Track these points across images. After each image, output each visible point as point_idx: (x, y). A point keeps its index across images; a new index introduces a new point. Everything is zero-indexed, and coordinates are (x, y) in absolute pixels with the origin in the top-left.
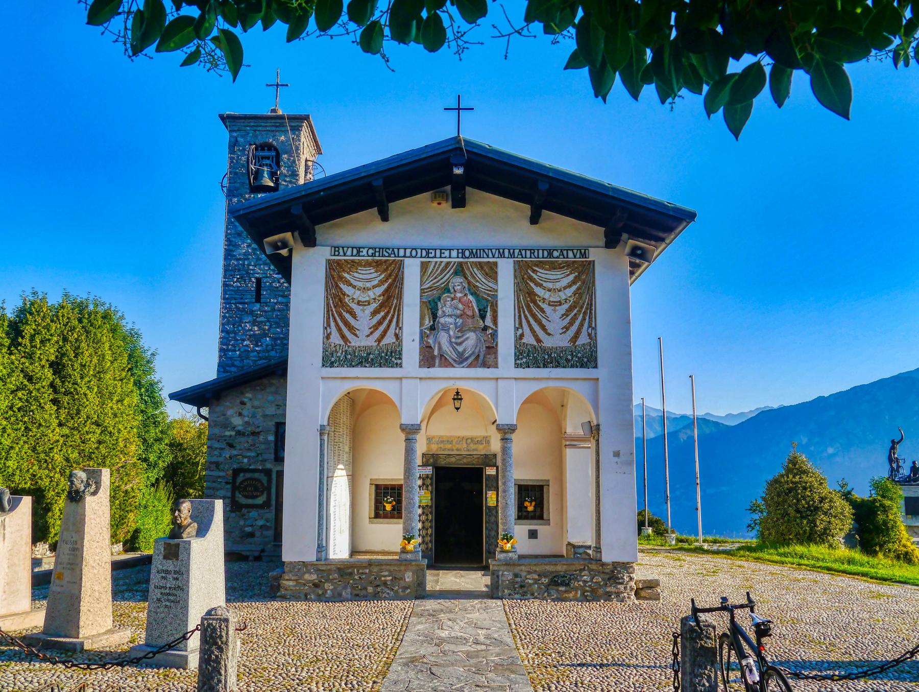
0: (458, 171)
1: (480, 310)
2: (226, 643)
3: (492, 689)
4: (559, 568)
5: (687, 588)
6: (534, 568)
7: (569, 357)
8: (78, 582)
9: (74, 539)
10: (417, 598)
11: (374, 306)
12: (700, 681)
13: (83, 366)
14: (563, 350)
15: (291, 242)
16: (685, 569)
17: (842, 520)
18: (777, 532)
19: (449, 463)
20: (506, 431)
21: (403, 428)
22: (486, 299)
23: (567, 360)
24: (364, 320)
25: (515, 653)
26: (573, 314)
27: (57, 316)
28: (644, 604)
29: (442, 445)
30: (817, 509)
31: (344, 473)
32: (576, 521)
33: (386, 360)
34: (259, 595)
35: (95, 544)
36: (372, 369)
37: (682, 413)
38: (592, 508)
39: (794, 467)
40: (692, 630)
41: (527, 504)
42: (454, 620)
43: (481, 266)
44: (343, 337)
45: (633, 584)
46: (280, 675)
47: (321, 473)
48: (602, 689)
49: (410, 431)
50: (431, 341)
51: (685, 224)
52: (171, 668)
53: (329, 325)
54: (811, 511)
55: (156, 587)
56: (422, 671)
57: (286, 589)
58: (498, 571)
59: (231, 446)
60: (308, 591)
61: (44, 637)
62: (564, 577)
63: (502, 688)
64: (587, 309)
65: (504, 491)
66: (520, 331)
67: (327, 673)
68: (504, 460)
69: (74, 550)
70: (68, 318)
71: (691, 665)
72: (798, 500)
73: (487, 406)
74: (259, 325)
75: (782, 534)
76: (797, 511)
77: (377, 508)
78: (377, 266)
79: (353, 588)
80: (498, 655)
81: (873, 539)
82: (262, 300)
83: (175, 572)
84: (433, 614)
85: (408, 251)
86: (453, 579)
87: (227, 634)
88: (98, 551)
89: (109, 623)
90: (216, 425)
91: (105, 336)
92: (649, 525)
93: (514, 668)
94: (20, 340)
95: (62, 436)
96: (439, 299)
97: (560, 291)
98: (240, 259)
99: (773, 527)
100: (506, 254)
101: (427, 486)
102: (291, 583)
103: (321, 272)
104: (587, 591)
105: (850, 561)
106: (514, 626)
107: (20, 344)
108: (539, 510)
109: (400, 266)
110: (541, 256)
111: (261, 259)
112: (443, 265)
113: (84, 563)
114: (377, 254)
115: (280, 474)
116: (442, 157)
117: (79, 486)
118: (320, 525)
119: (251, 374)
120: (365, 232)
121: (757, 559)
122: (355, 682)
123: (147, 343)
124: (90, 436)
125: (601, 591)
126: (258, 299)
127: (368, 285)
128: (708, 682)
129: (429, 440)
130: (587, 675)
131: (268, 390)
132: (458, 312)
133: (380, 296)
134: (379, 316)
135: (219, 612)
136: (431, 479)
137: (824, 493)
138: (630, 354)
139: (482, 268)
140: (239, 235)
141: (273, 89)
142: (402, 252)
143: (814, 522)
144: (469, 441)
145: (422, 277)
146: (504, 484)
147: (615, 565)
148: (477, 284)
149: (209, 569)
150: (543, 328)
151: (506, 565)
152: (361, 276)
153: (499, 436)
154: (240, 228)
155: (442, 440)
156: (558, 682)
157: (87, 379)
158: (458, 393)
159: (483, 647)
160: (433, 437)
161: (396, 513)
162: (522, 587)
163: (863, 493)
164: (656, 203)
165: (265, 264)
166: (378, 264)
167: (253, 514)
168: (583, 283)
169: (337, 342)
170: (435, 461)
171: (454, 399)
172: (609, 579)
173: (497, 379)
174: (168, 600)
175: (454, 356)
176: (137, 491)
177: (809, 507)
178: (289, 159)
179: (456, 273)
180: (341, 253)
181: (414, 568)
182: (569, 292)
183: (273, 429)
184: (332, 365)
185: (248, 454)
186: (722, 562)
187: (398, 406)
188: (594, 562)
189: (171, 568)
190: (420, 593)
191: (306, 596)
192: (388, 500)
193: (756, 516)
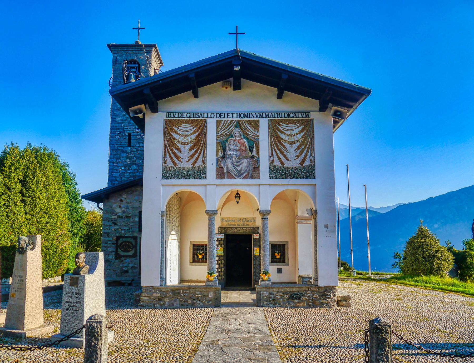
0: (237, 69)
1: (249, 147)
2: (101, 336)
3: (258, 361)
4: (294, 290)
5: (365, 300)
6: (281, 290)
7: (300, 173)
8: (23, 299)
9: (21, 275)
10: (216, 306)
11: (191, 145)
12: (382, 358)
13: (37, 182)
14: (296, 168)
15: (144, 110)
16: (362, 289)
17: (448, 262)
18: (412, 269)
19: (234, 232)
20: (265, 214)
21: (207, 213)
22: (253, 141)
23: (298, 174)
24: (185, 153)
25: (270, 339)
26: (301, 149)
27: (24, 156)
28: (342, 309)
29: (229, 223)
30: (434, 256)
31: (175, 237)
32: (303, 264)
33: (198, 175)
34: (128, 305)
35: (33, 277)
36: (190, 180)
37: (357, 206)
38: (311, 257)
39: (421, 234)
40: (377, 328)
41: (276, 254)
42: (235, 319)
43: (250, 122)
44: (174, 162)
45: (335, 298)
46: (136, 352)
47: (162, 238)
48: (322, 361)
49: (211, 214)
50: (222, 164)
51: (365, 97)
52: (74, 348)
53: (166, 156)
54: (431, 258)
55: (66, 302)
56: (217, 350)
57: (143, 302)
58: (261, 291)
59: (115, 224)
60: (155, 303)
61: (4, 329)
62: (297, 294)
63: (263, 360)
64: (309, 146)
65: (264, 247)
66: (272, 159)
67: (163, 351)
68: (263, 230)
69: (21, 280)
70: (29, 157)
71: (376, 349)
72: (424, 252)
73: (254, 201)
74: (130, 158)
75: (415, 270)
76: (423, 258)
77: (194, 257)
78: (192, 123)
79: (180, 301)
80: (261, 339)
81: (465, 273)
82: (132, 145)
83: (76, 293)
84: (224, 316)
85: (209, 115)
86: (236, 295)
87: (101, 330)
88: (35, 281)
89: (42, 321)
90: (107, 213)
91: (49, 166)
92: (345, 267)
93: (270, 347)
94: (3, 168)
95: (27, 219)
96: (227, 141)
97: (294, 136)
98: (119, 123)
99: (410, 266)
100: (264, 116)
101: (221, 245)
102: (146, 298)
103: (160, 127)
104: (310, 302)
105: (453, 285)
106: (270, 322)
107: (4, 171)
108: (282, 258)
109: (205, 123)
110: (283, 116)
111: (131, 123)
112: (229, 122)
113: (27, 288)
114: (192, 116)
115: (141, 238)
116: (229, 60)
117: (23, 245)
118: (162, 266)
119: (125, 185)
120: (185, 104)
121: (402, 284)
122: (178, 357)
123: (71, 169)
124: (42, 219)
125: (318, 302)
126: (129, 145)
127: (187, 133)
128: (386, 358)
129: (222, 219)
130: (313, 352)
131: (135, 193)
132: (238, 148)
133: (194, 140)
134: (193, 151)
135: (96, 318)
136: (224, 241)
137: (438, 248)
138: (333, 171)
139: (251, 123)
140: (118, 110)
141: (136, 30)
142: (206, 115)
143: (432, 263)
144: (244, 220)
145: (217, 129)
146: (264, 243)
147: (326, 288)
148: (248, 132)
149: (96, 292)
150: (285, 156)
151: (265, 288)
152: (183, 129)
153: (261, 217)
154: (119, 106)
155: (229, 220)
156: (296, 356)
157: (39, 189)
158: (238, 194)
159: (252, 335)
160: (225, 218)
161: (204, 260)
162: (274, 300)
163: (459, 248)
164: (348, 85)
165: (133, 125)
166: (192, 122)
167: (128, 260)
168: (307, 131)
169: (170, 165)
170: (226, 231)
171: (236, 197)
172: (322, 296)
173: (259, 185)
174: (72, 309)
175: (236, 172)
176: (68, 248)
177: (430, 255)
178: (145, 68)
179: (236, 126)
180: (172, 116)
181: (214, 290)
182: (299, 136)
183: (138, 214)
184: (167, 178)
185: (125, 228)
186: (382, 285)
187: (205, 200)
188: (314, 286)
189: (74, 291)
190: (217, 304)
191: (154, 305)
192: (200, 252)
193: (397, 260)
